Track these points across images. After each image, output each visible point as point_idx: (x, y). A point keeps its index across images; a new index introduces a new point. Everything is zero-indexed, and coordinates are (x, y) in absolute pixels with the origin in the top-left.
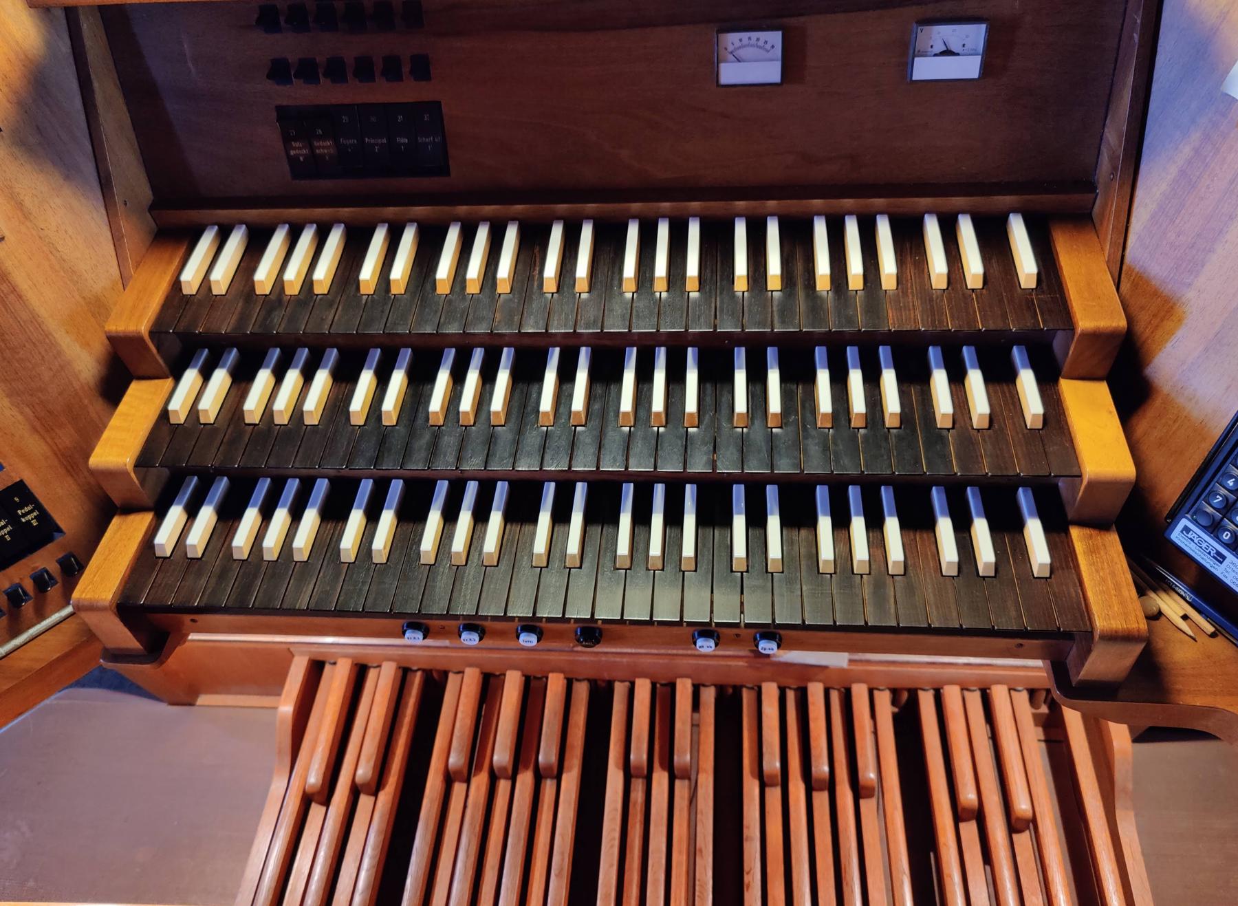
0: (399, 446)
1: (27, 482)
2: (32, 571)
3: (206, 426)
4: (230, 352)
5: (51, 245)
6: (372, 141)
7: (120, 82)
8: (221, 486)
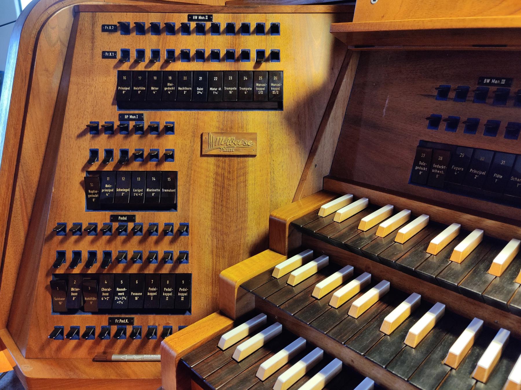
0: (412, 364)
1: (193, 276)
2: (166, 324)
3: (289, 286)
4: (324, 257)
5: (273, 169)
6: (475, 171)
7: (345, 114)
8: (276, 329)
